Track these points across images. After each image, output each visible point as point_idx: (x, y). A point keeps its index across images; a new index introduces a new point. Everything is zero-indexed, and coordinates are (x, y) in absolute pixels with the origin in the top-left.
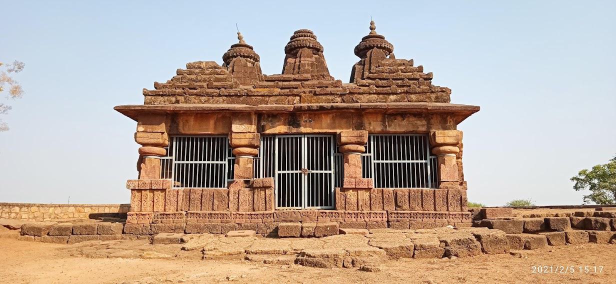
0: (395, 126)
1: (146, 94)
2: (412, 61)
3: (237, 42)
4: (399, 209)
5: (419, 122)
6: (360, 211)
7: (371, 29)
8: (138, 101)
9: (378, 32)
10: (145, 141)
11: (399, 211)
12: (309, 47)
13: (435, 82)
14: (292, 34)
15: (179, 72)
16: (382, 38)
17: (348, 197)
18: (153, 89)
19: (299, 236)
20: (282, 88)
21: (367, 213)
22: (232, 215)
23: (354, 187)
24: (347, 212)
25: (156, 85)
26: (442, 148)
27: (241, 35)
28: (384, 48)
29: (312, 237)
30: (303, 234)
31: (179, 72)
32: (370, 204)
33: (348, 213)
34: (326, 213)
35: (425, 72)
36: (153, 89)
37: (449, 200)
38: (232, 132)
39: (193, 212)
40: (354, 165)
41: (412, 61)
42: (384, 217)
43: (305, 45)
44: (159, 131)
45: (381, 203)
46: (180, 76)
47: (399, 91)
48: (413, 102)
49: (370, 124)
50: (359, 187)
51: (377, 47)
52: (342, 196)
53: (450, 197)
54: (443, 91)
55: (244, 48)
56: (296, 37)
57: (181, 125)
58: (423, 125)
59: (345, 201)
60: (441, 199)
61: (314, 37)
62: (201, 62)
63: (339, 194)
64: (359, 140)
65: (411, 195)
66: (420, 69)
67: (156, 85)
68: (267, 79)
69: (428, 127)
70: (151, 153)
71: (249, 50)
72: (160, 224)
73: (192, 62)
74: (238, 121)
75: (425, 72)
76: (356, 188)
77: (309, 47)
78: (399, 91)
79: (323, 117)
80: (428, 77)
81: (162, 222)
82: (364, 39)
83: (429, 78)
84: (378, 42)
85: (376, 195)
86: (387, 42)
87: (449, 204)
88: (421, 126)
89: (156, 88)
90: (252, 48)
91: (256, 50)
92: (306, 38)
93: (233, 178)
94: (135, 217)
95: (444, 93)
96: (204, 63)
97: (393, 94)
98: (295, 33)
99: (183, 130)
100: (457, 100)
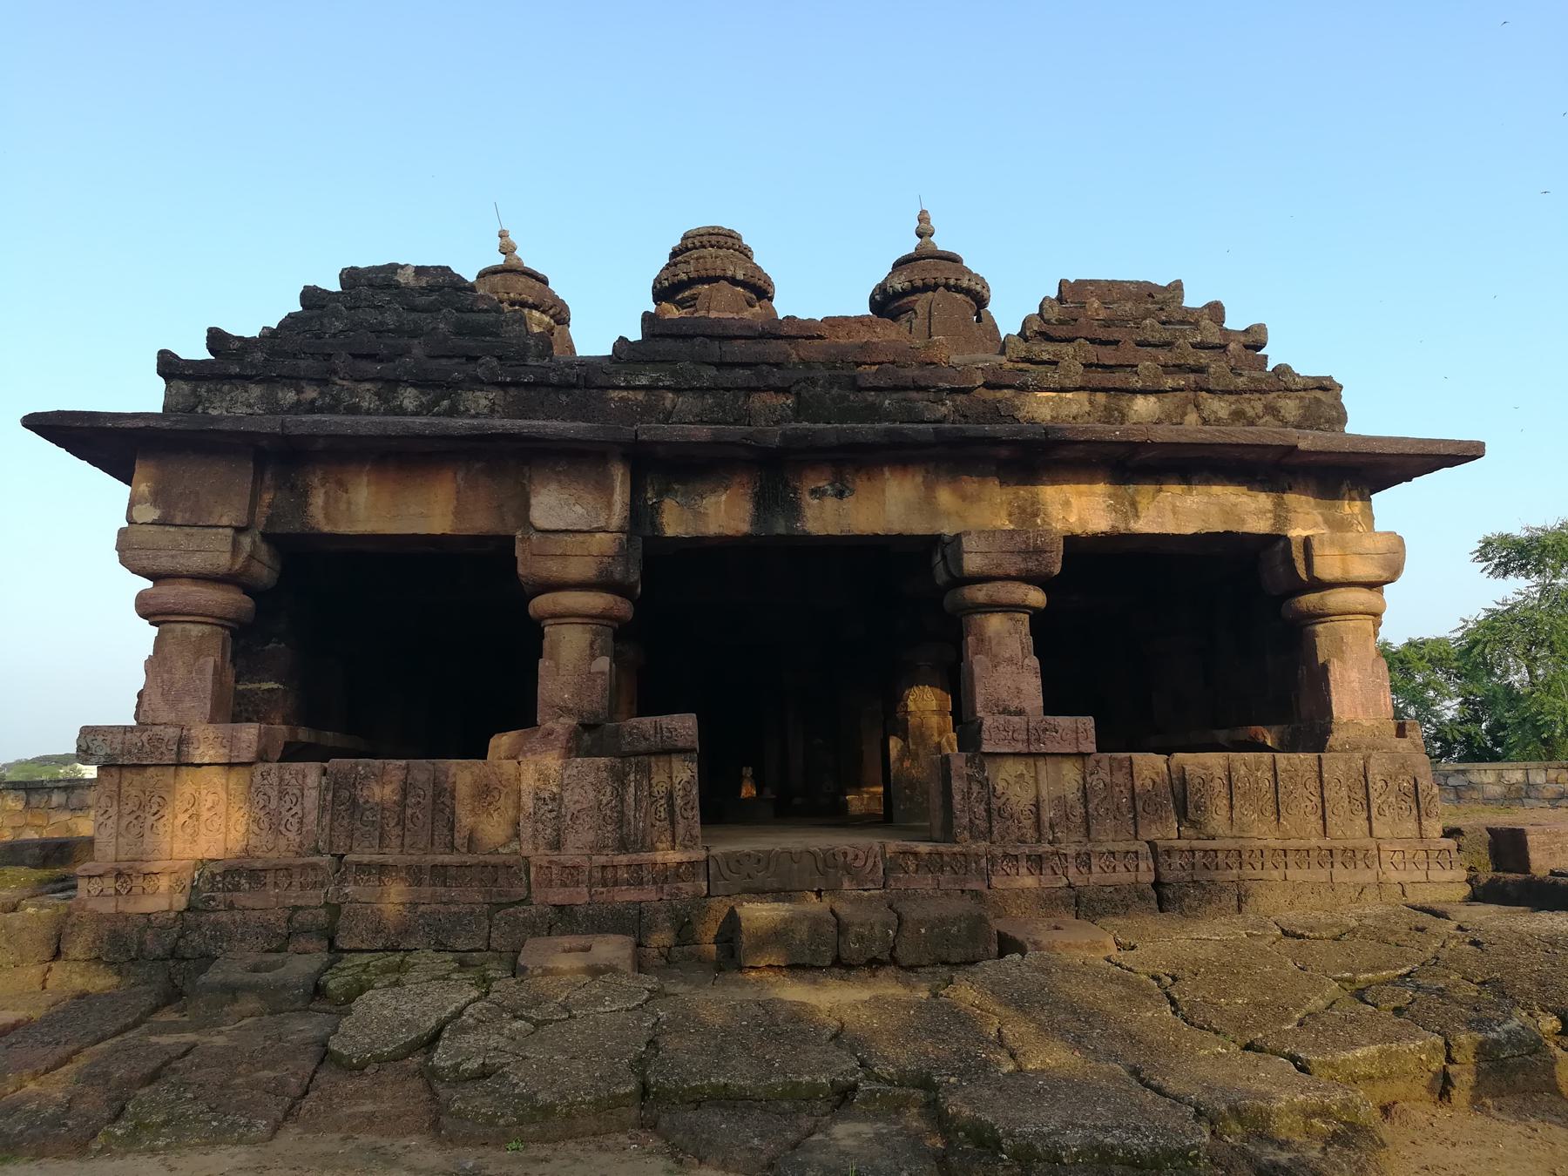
0: (1160, 513)
1: (169, 365)
2: (1177, 286)
3: (500, 260)
4: (1191, 832)
5: (1245, 499)
6: (1047, 847)
7: (920, 235)
8: (146, 396)
9: (942, 242)
10: (164, 563)
11: (1196, 844)
12: (734, 281)
13: (1275, 354)
14: (677, 242)
15: (311, 296)
16: (953, 259)
17: (999, 789)
18: (204, 354)
19: (828, 963)
20: (720, 365)
21: (1078, 855)
22: (533, 869)
23: (1021, 747)
24: (998, 851)
25: (216, 338)
26: (980, 593)
27: (512, 237)
28: (968, 292)
29: (882, 964)
30: (844, 955)
31: (311, 296)
32: (1087, 818)
33: (1006, 855)
34: (916, 854)
35: (1235, 321)
36: (204, 354)
37: (1373, 795)
38: (525, 521)
39: (366, 859)
40: (1011, 661)
41: (1177, 286)
42: (1143, 866)
43: (719, 273)
44: (225, 521)
45: (1124, 810)
46: (317, 312)
47: (1169, 382)
48: (1210, 419)
49: (1067, 504)
50: (1043, 748)
51: (948, 287)
52: (975, 788)
53: (1377, 784)
54: (1324, 389)
55: (523, 279)
56: (688, 250)
57: (318, 500)
58: (1261, 513)
59: (988, 804)
60: (1344, 792)
61: (746, 252)
62: (394, 268)
63: (961, 777)
64: (1032, 565)
65: (1234, 779)
66: (1216, 311)
67: (216, 338)
68: (657, 331)
69: (1277, 517)
70: (173, 613)
71: (538, 285)
72: (224, 917)
73: (363, 264)
74: (553, 486)
75: (1235, 321)
76: (1029, 755)
77: (734, 281)
78: (1169, 382)
79: (887, 474)
80: (1250, 340)
81: (231, 907)
82: (900, 265)
83: (1254, 340)
84: (942, 273)
85: (1108, 780)
86: (970, 272)
87: (1374, 811)
88: (1245, 510)
89: (211, 351)
90: (544, 281)
91: (557, 287)
92: (721, 252)
93: (948, 835)
94: (109, 884)
95: (147, 608)
96: (410, 272)
97: (1145, 392)
98: (685, 237)
99: (327, 516)
100: (1369, 418)
